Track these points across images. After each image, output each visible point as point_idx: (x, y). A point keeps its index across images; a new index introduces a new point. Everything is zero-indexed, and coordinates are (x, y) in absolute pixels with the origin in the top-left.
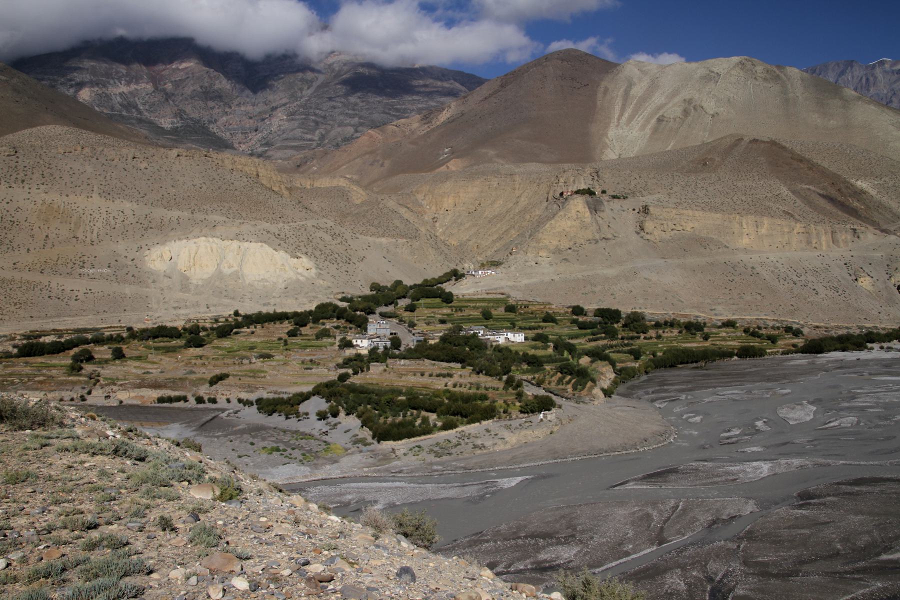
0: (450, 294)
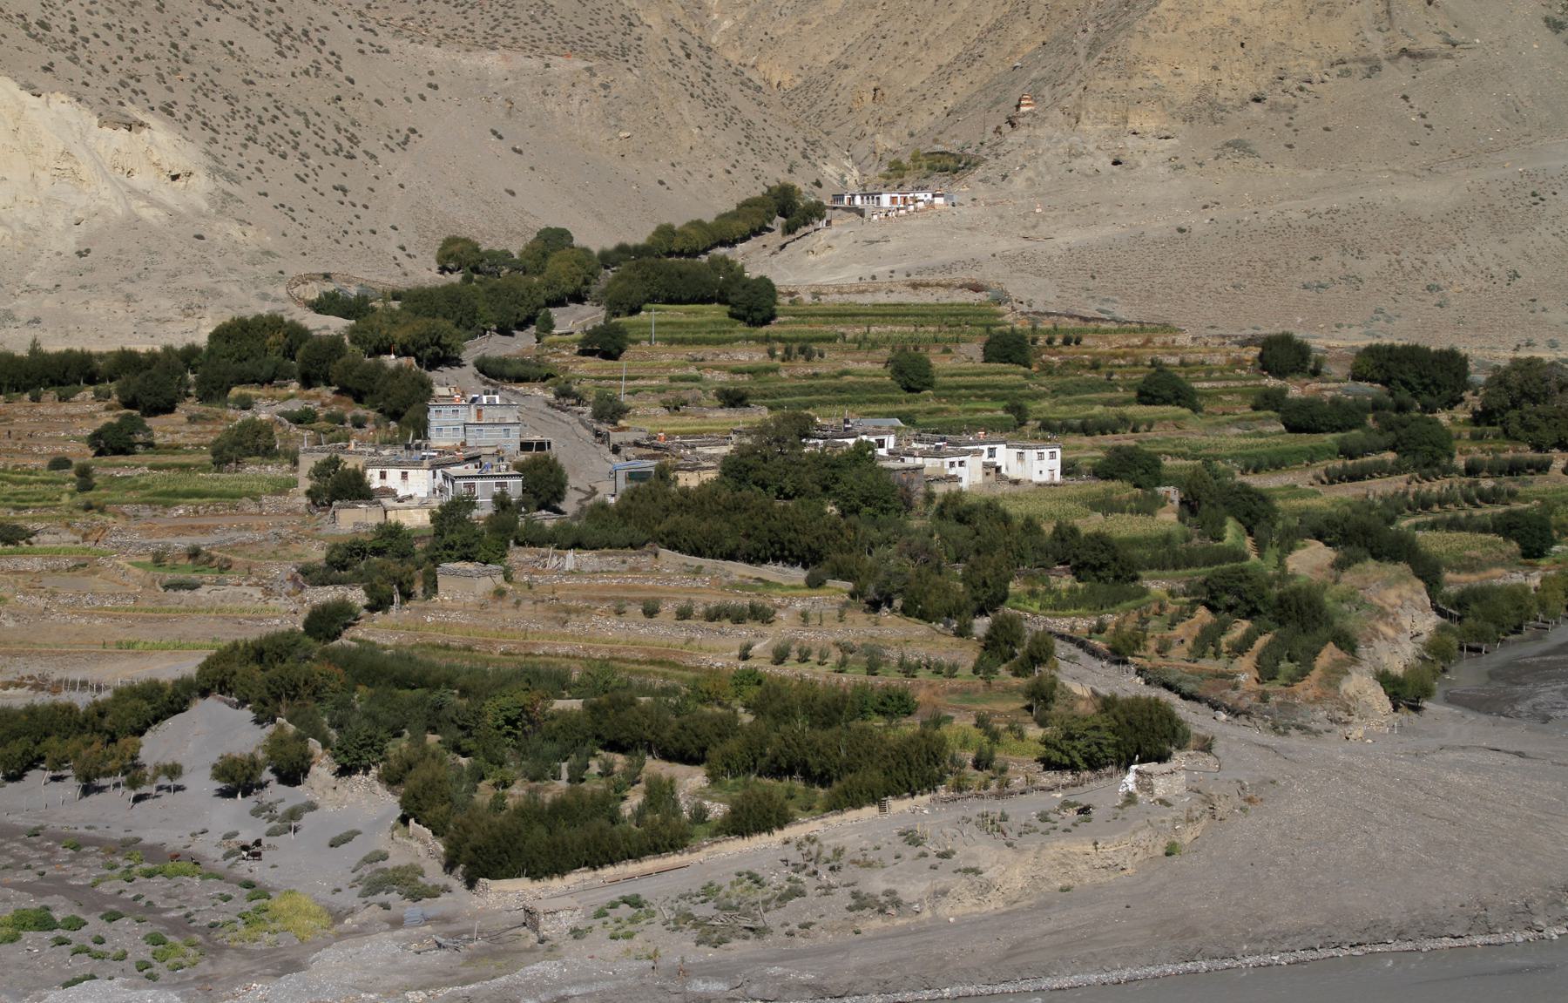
0: (765, 288)
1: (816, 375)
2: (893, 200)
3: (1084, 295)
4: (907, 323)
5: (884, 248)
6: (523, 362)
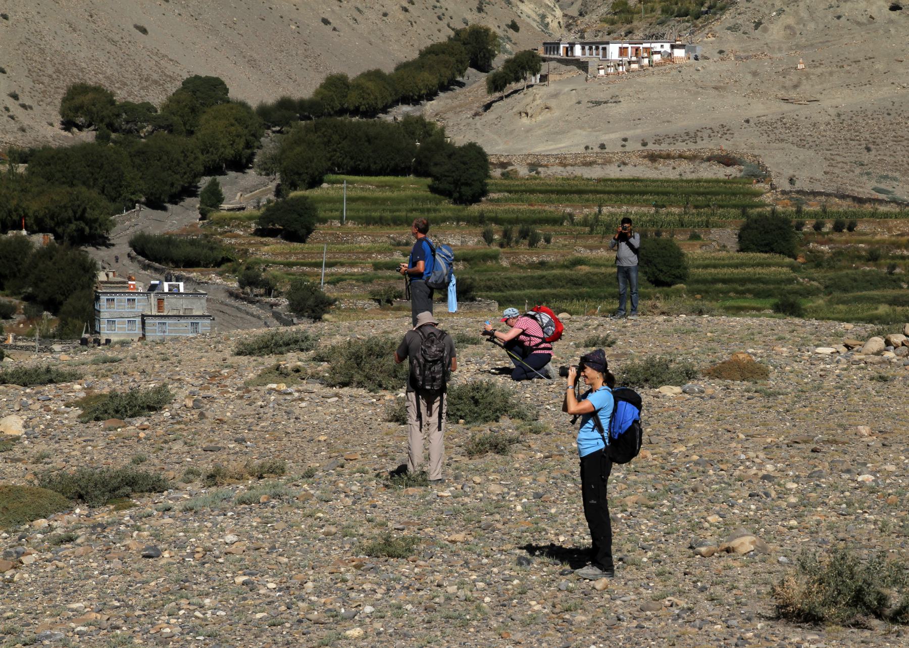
0: (474, 155)
1: (542, 264)
2: (623, 52)
3: (858, 171)
4: (647, 203)
5: (613, 110)
6: (193, 243)
